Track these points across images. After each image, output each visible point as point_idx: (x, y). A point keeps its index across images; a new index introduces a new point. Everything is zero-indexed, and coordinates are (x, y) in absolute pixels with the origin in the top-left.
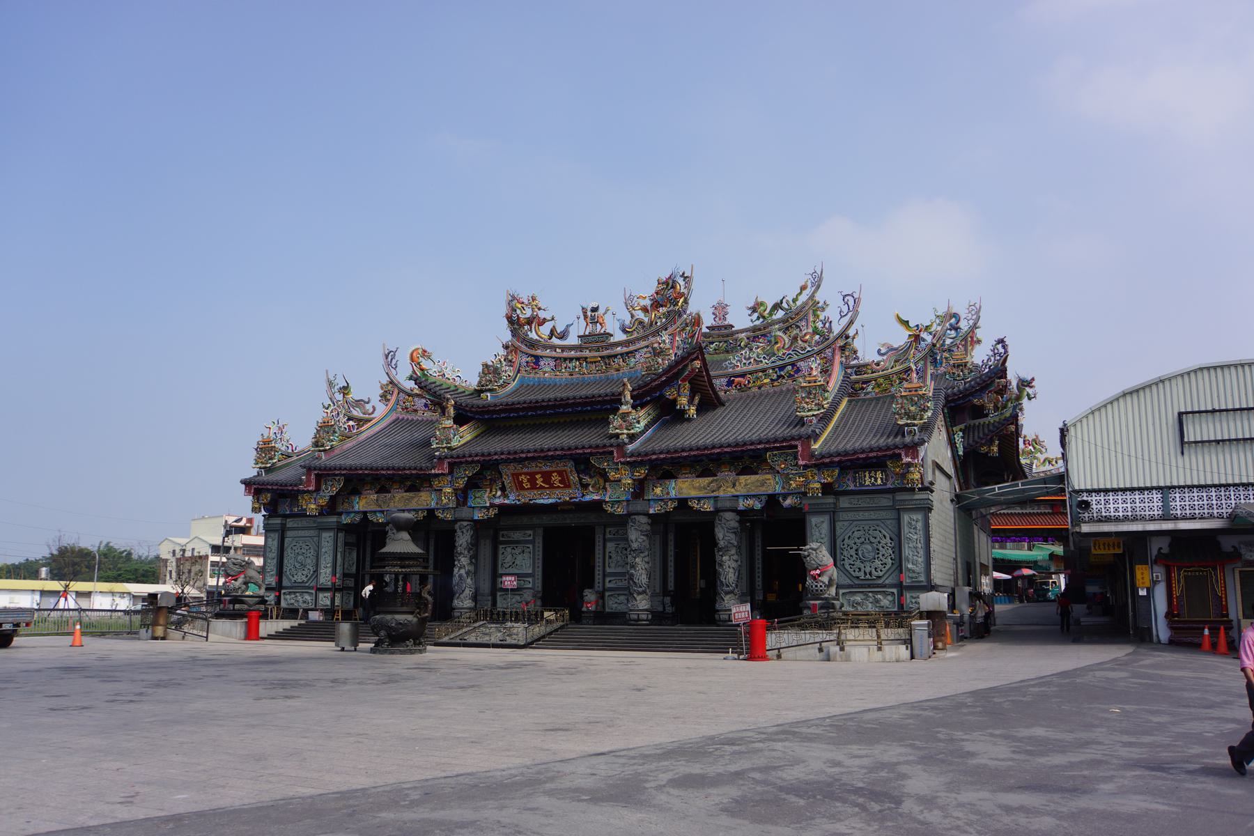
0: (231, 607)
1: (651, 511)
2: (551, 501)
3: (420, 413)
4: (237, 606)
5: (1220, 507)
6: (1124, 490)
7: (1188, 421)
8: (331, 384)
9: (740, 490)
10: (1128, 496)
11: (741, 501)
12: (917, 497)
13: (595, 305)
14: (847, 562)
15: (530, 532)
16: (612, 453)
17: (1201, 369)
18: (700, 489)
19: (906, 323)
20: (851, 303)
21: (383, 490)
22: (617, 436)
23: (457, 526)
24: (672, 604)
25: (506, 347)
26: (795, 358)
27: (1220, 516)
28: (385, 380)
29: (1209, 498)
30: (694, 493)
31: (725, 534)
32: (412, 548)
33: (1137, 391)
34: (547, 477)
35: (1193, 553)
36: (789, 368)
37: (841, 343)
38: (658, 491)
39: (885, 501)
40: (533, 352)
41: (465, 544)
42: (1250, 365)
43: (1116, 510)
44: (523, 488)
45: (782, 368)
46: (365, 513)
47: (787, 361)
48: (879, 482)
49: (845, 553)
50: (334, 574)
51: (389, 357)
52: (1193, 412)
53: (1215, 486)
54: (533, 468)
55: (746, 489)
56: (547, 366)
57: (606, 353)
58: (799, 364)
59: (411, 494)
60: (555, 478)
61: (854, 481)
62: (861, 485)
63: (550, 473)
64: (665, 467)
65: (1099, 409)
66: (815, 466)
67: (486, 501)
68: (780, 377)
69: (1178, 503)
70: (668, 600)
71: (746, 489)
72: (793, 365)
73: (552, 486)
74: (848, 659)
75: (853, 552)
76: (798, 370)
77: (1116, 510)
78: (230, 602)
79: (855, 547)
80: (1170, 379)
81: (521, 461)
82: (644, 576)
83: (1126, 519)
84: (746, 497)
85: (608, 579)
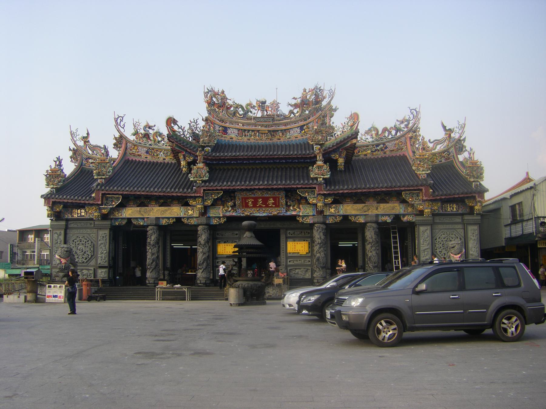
1: (327, 222)
2: (264, 214)
8: (72, 134)
9: (380, 212)
15: (237, 232)
16: (315, 188)
18: (357, 210)
19: (444, 127)
20: (415, 113)
22: (316, 179)
26: (385, 140)
30: (354, 213)
31: (152, 238)
36: (382, 146)
38: (332, 210)
39: (458, 219)
40: (223, 124)
46: (129, 220)
47: (380, 142)
51: (118, 121)
54: (259, 194)
55: (387, 210)
58: (387, 144)
60: (271, 201)
61: (442, 209)
63: (268, 199)
67: (219, 213)
70: (166, 272)
71: (387, 210)
72: (384, 144)
73: (267, 206)
75: (441, 245)
76: (386, 148)
79: (442, 243)
84: (383, 215)
85: (289, 260)
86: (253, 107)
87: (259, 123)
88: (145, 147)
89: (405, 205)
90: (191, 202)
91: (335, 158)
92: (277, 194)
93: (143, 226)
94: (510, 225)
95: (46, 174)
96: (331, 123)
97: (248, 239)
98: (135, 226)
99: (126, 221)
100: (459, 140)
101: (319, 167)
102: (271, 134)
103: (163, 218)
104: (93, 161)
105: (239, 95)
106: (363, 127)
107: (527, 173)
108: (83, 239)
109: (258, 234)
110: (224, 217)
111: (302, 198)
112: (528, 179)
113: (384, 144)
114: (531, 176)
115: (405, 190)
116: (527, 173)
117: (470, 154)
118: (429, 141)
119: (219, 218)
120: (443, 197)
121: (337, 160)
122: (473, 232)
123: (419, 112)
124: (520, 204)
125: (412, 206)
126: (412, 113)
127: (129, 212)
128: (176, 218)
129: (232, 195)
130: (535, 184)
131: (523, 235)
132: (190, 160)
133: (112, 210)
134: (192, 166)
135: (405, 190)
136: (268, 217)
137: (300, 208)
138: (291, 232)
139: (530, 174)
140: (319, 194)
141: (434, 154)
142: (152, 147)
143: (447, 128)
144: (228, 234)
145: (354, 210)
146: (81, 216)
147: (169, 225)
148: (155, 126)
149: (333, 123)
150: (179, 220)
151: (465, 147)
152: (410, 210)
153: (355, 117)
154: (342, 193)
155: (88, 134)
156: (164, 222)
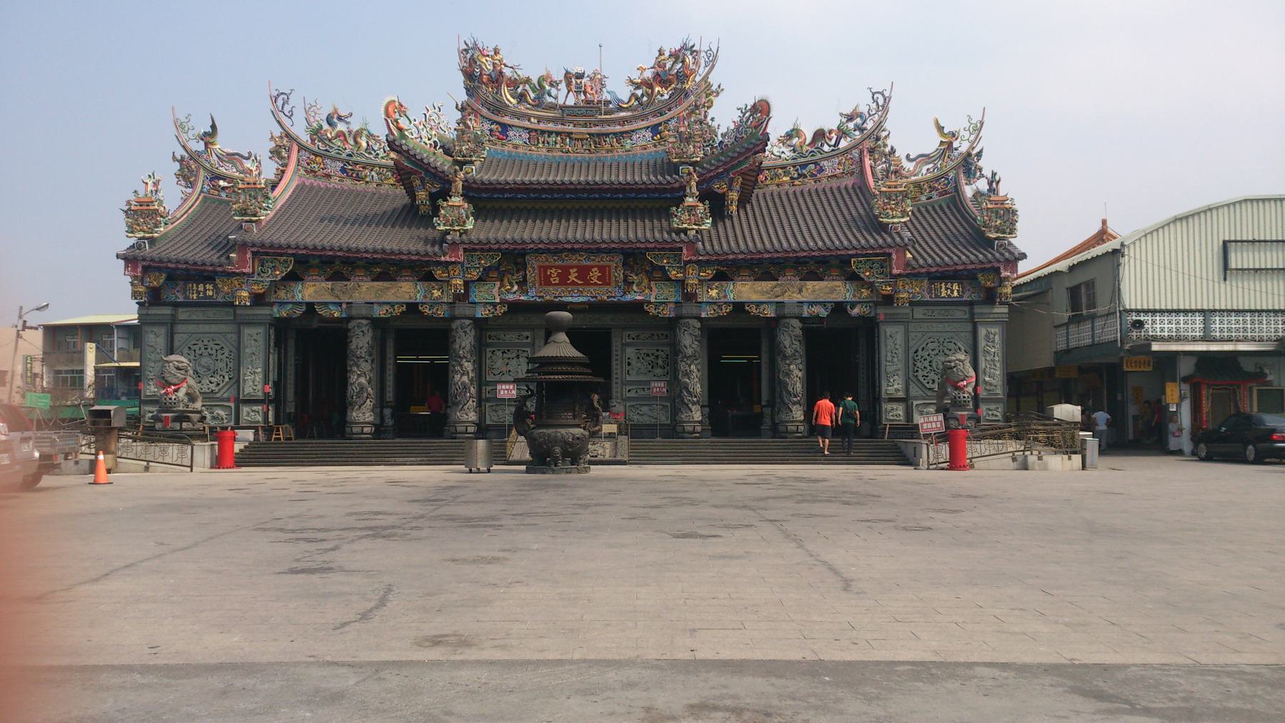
0: (177, 426)
1: (703, 315)
2: (581, 299)
3: (335, 180)
4: (185, 425)
5: (1253, 330)
6: (1170, 312)
7: (1232, 247)
8: (179, 126)
9: (806, 296)
10: (1174, 318)
11: (805, 307)
12: (996, 310)
13: (579, 70)
14: (920, 374)
15: (528, 334)
16: (681, 249)
17: (1246, 201)
18: (763, 293)
19: (940, 129)
20: (881, 102)
21: (337, 277)
22: (685, 231)
23: (351, 325)
24: (393, 415)
25: (462, 109)
26: (819, 156)
27: (1269, 340)
28: (277, 131)
29: (1245, 322)
30: (755, 298)
31: (361, 341)
32: (570, 351)
33: (1187, 217)
34: (584, 272)
35: (1218, 371)
37: (869, 144)
38: (714, 293)
39: (960, 313)
41: (468, 348)
42: (1281, 200)
43: (1162, 330)
44: (550, 284)
45: (804, 166)
46: (310, 306)
48: (956, 294)
49: (919, 364)
50: (266, 382)
51: (280, 101)
52: (1236, 241)
53: (1251, 311)
54: (574, 260)
56: (517, 138)
57: (595, 130)
59: (386, 284)
60: (595, 273)
61: (930, 292)
62: (936, 296)
64: (726, 270)
65: (1151, 233)
66: (908, 276)
67: (491, 297)
68: (800, 176)
69: (1217, 324)
70: (387, 412)
72: (816, 163)
73: (587, 283)
74: (1045, 468)
75: (926, 364)
76: (821, 170)
77: (1162, 330)
78: (175, 420)
80: (1217, 208)
81: (556, 252)
82: (798, 385)
83: (1170, 339)
84: (811, 304)
86: (553, 84)
87: (571, 118)
88: (339, 160)
89: (855, 283)
90: (438, 273)
91: (720, 191)
92: (605, 260)
93: (340, 320)
94: (1067, 325)
95: (126, 208)
96: (709, 119)
97: (562, 347)
98: (322, 319)
99: (304, 308)
100: (969, 155)
101: (691, 209)
102: (595, 143)
103: (380, 304)
104: (226, 184)
105: (531, 56)
106: (776, 128)
107: (1104, 222)
108: (211, 344)
109: (576, 337)
110: (503, 302)
111: (655, 268)
112: (1102, 235)
113: (816, 163)
114: (1112, 227)
115: (857, 256)
116: (1104, 222)
117: (990, 184)
118: (908, 156)
119: (494, 305)
120: (933, 270)
121: (724, 195)
122: (992, 340)
123: (890, 98)
124: (1090, 285)
125: (871, 286)
126: (875, 101)
127: (310, 291)
128: (407, 304)
129: (520, 260)
130: (1122, 245)
131: (1093, 345)
132: (434, 190)
133: (275, 286)
134: (440, 202)
135: (857, 256)
136: (589, 303)
137: (651, 289)
138: (633, 334)
139: (1109, 224)
140: (690, 262)
141: (917, 185)
142: (354, 159)
143: (946, 131)
144: (511, 337)
145: (756, 292)
146: (206, 297)
147: (394, 318)
148: (351, 115)
149: (712, 119)
150: (412, 308)
151: (981, 170)
152: (865, 293)
153: (761, 110)
154: (734, 260)
155: (214, 127)
156: (380, 312)
